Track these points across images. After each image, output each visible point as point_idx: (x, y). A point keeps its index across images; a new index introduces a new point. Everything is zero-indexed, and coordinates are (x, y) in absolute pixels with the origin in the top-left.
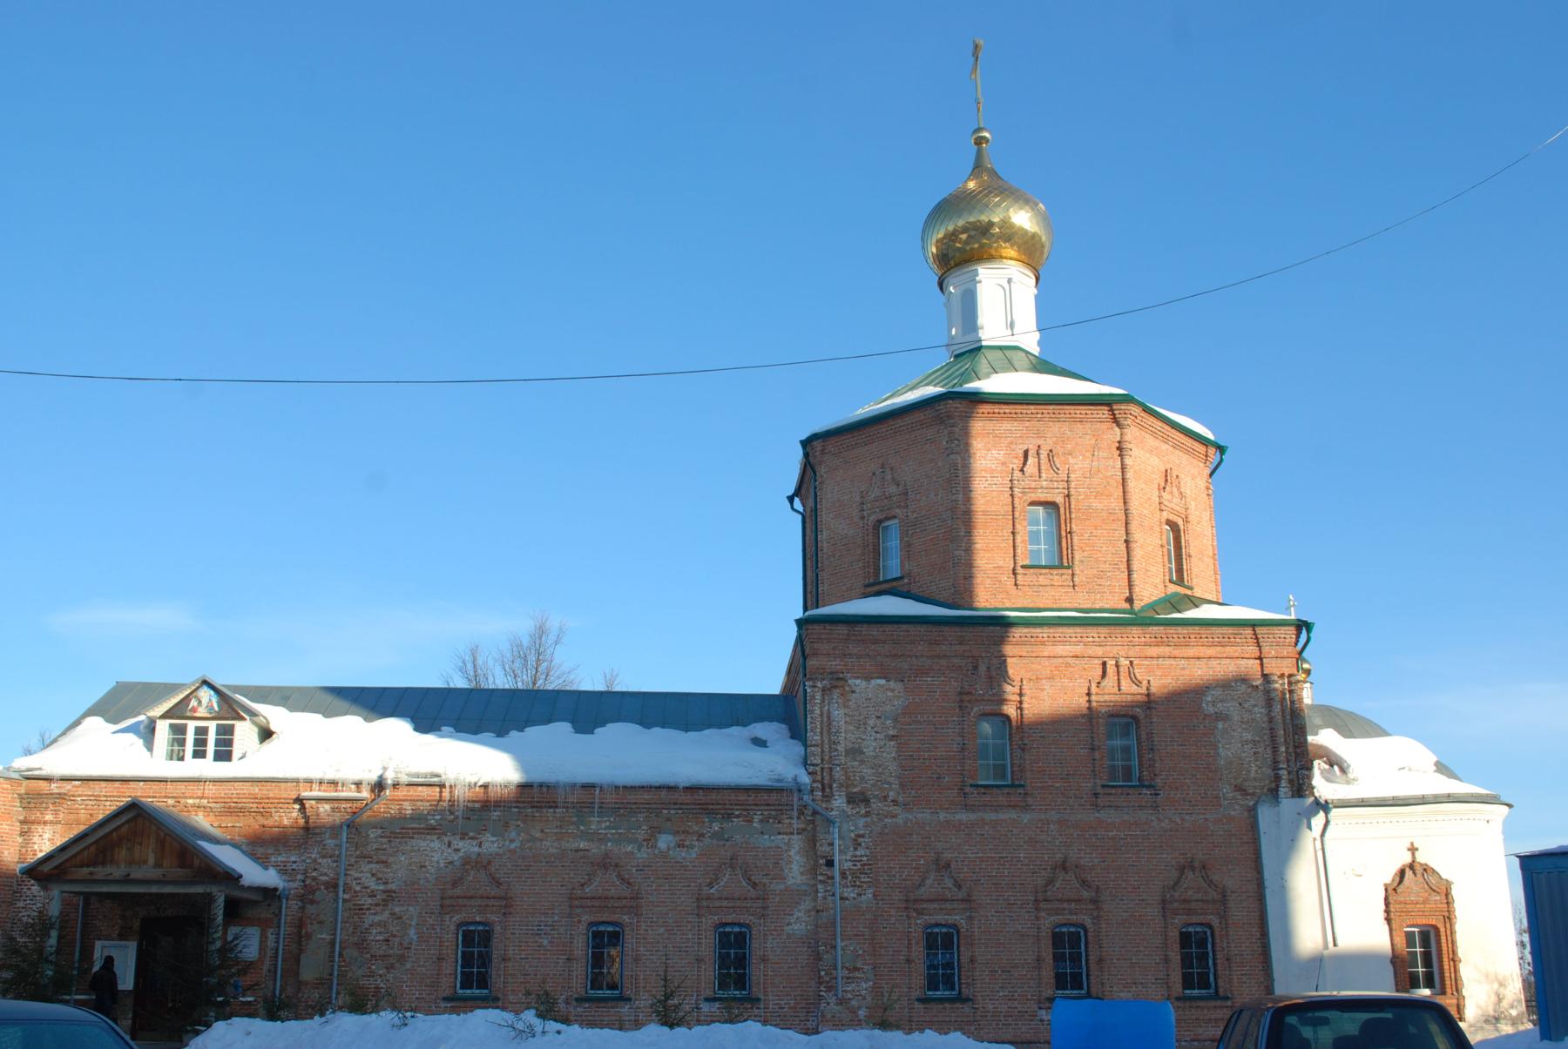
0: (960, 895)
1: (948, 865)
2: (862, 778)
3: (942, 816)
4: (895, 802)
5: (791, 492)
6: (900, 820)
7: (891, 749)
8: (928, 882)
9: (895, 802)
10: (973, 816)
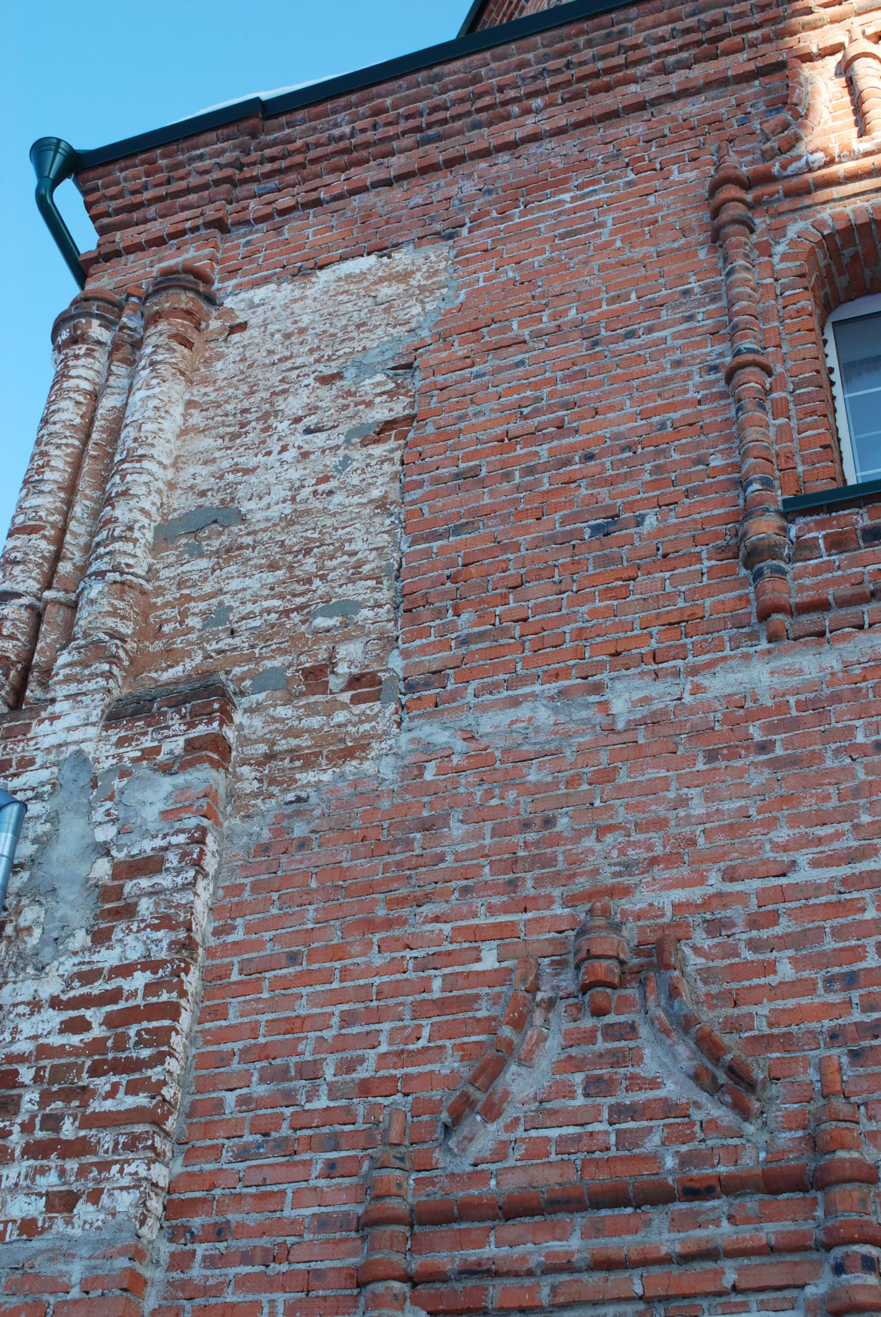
0: (759, 1144)
1: (656, 956)
2: (218, 618)
3: (624, 698)
4: (364, 684)
5: (86, 140)
6: (380, 767)
7: (377, 470)
8: (521, 1084)
9: (364, 684)
10: (813, 664)
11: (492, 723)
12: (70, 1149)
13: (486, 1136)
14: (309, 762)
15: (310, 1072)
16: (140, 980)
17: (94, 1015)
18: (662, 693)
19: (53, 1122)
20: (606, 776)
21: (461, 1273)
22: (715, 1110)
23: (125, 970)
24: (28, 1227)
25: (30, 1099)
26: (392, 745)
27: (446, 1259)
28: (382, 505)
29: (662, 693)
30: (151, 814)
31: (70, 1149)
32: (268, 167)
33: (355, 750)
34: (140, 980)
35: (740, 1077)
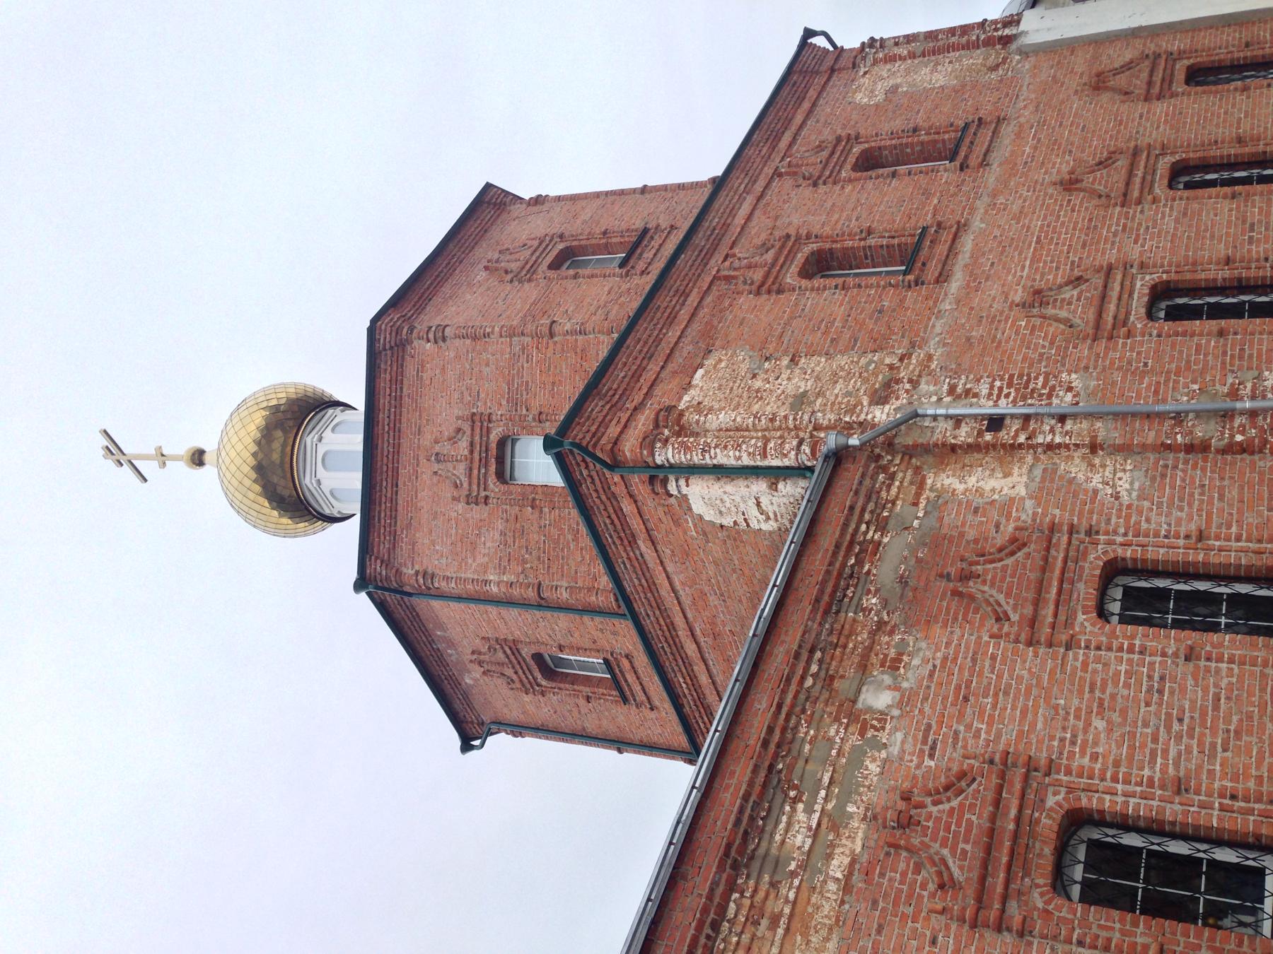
0: (1098, 281)
8: (1063, 314)
12: (1053, 388)
17: (1006, 391)
22: (1084, 287)
23: (992, 387)
27: (1110, 319)
30: (932, 388)
35: (1079, 278)
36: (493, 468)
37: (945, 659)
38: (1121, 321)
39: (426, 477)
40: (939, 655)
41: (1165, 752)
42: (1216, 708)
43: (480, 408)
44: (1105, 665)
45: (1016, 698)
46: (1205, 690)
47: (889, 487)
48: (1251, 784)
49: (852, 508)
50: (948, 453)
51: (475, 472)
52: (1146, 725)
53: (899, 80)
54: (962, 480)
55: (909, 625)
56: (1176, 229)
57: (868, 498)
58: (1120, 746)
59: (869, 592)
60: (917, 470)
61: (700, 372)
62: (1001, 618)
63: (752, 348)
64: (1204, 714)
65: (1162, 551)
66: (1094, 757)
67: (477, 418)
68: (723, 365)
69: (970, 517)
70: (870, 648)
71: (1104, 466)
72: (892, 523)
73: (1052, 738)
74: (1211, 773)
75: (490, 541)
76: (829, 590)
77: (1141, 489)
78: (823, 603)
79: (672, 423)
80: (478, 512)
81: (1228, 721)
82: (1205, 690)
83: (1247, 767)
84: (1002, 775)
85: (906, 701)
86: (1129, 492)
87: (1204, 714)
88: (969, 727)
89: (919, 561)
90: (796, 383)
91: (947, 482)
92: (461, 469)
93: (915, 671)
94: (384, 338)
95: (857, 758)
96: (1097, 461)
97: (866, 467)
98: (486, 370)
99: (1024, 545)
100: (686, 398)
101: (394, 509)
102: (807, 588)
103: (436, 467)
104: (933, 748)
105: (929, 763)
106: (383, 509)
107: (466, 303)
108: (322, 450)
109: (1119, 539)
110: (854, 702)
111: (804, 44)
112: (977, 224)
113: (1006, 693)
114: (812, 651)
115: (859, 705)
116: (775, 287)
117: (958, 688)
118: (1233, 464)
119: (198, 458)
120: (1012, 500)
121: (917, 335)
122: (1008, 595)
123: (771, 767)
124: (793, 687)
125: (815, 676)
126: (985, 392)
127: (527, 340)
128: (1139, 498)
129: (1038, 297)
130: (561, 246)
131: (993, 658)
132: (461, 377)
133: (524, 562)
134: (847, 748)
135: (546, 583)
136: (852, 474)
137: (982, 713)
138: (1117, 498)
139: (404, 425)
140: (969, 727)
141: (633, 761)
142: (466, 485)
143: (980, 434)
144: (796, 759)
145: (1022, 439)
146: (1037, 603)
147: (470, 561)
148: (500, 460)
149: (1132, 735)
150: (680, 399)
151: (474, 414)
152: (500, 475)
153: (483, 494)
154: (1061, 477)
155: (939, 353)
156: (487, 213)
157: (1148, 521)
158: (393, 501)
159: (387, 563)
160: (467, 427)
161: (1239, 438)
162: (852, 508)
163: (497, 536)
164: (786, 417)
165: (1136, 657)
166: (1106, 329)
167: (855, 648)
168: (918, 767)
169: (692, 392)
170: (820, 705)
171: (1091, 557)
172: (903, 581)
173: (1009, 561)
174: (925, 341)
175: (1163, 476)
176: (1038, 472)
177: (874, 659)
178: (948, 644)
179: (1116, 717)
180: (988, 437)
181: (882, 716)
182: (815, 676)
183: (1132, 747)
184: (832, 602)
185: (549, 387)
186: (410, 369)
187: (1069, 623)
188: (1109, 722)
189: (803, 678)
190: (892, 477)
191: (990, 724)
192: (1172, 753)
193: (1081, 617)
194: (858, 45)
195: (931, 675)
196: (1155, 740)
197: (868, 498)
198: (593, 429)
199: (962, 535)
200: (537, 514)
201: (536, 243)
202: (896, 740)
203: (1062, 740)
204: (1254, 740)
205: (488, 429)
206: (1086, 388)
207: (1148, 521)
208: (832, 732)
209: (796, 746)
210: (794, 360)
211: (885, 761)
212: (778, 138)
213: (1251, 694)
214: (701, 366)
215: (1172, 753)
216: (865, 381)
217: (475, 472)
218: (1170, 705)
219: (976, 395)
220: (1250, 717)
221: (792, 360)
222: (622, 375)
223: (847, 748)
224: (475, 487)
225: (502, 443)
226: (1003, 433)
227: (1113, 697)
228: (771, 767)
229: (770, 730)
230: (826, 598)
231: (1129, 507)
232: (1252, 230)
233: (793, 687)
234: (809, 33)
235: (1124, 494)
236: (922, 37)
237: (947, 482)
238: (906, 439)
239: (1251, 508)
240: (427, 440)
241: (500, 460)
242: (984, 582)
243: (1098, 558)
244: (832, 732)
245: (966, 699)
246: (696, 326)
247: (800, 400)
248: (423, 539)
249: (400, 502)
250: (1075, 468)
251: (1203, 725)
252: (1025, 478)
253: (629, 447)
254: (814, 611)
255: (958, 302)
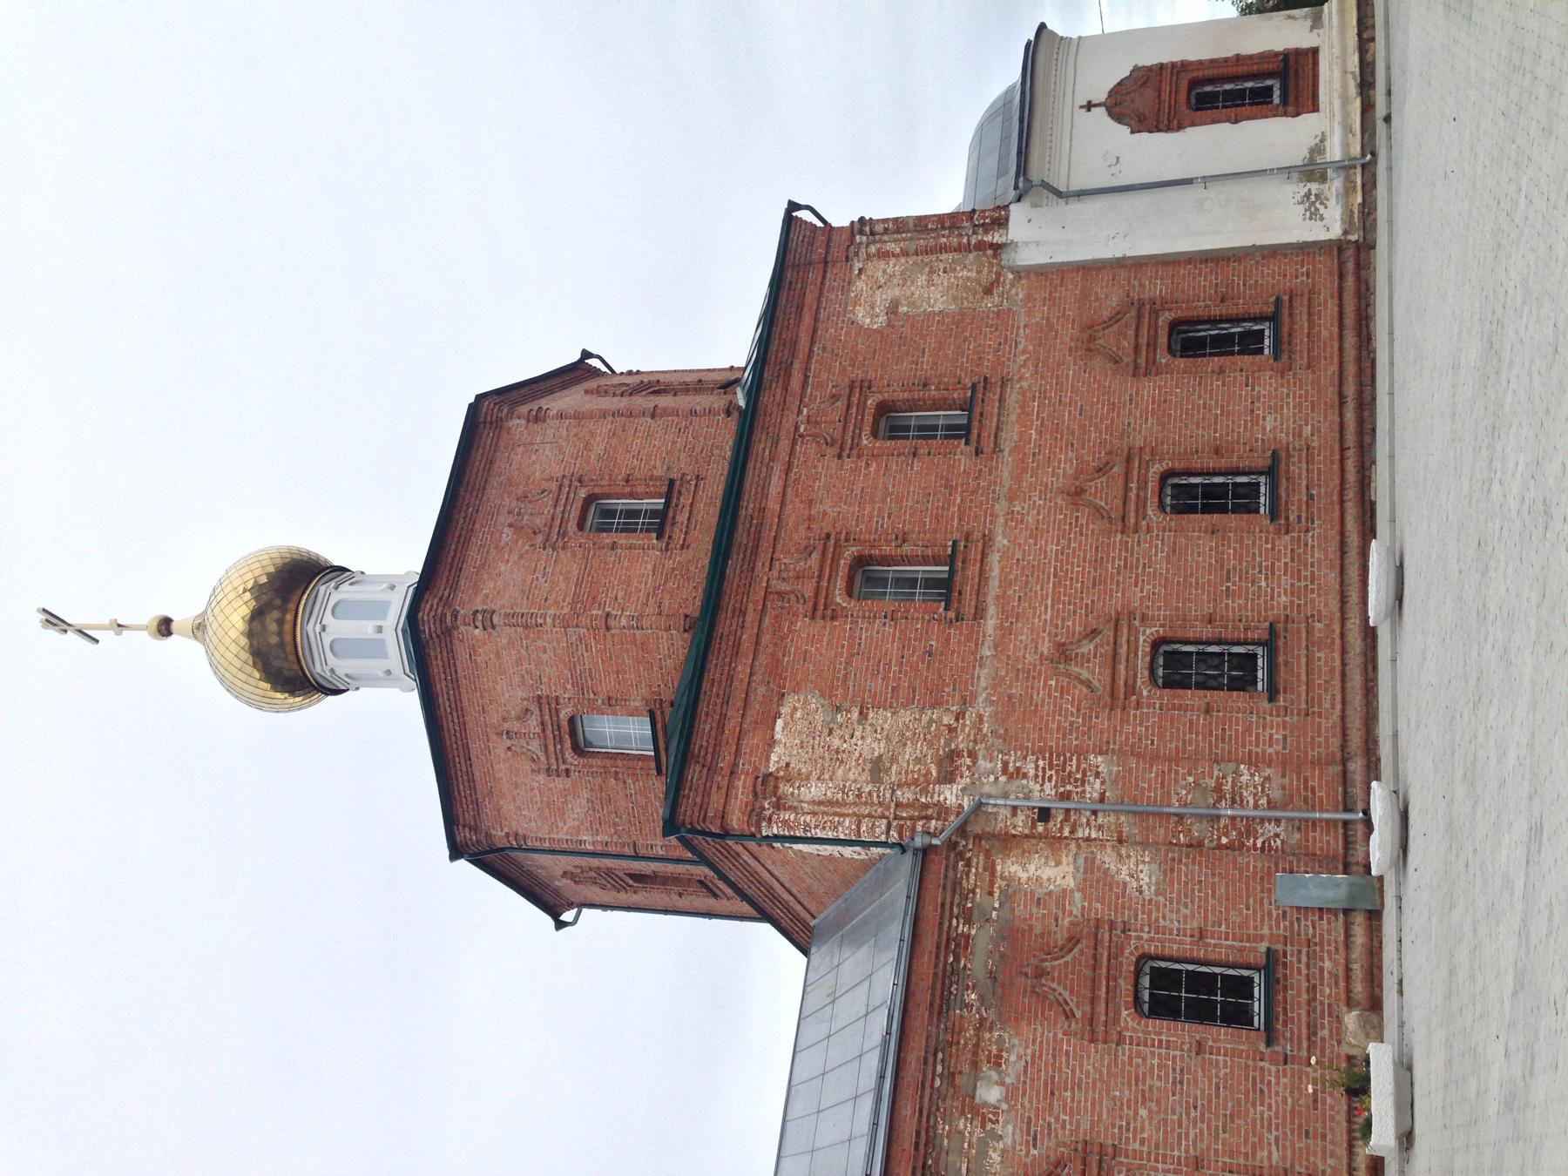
0: (1108, 633)
3: (987, 652)
8: (1085, 675)
10: (992, 610)
11: (983, 683)
12: (1084, 774)
13: (1096, 683)
14: (980, 730)
15: (1072, 724)
16: (1041, 763)
17: (1048, 773)
18: (989, 642)
19: (1076, 780)
20: (1008, 657)
21: (701, 882)
22: (1098, 640)
23: (1037, 767)
24: (1103, 783)
25: (1069, 787)
26: (982, 706)
27: (1122, 690)
28: (894, 713)
29: (989, 642)
30: (989, 765)
31: (1084, 774)
32: (926, 1105)
33: (980, 717)
34: (1041, 763)
35: (1093, 631)
36: (568, 744)
37: (1033, 1055)
38: (1131, 689)
39: (500, 751)
40: (1029, 1051)
41: (1187, 1135)
42: (1217, 1097)
43: (544, 690)
44: (1144, 1059)
45: (1087, 1092)
46: (1210, 1081)
47: (968, 874)
48: (1242, 1161)
49: (943, 905)
50: (1007, 841)
51: (551, 748)
52: (1173, 1113)
53: (897, 292)
54: (1025, 869)
55: (1004, 1021)
56: (1168, 570)
57: (954, 891)
58: (1158, 1130)
59: (968, 987)
60: (988, 853)
61: (780, 723)
62: (1069, 1015)
63: (823, 695)
64: (1210, 1101)
65: (1175, 947)
66: (1142, 1142)
67: (544, 701)
68: (799, 714)
69: (1035, 910)
70: (977, 1046)
71: (1129, 857)
72: (976, 913)
73: (1114, 1126)
74: (1216, 1151)
75: (578, 808)
76: (938, 993)
77: (1157, 883)
78: (936, 1006)
79: (766, 784)
80: (559, 783)
81: (1225, 1109)
82: (1210, 1081)
83: (1238, 1146)
84: (1084, 1163)
85: (1011, 1094)
86: (1149, 885)
87: (1210, 1101)
88: (1057, 1119)
89: (1002, 955)
90: (871, 746)
91: (1013, 869)
92: (535, 745)
93: (1014, 1063)
94: (428, 627)
95: (983, 1146)
96: (1123, 851)
97: (947, 858)
98: (545, 657)
99: (1078, 941)
100: (774, 758)
101: (471, 780)
102: (923, 996)
103: (509, 743)
104: (1035, 1139)
105: (1034, 1152)
106: (462, 787)
107: (505, 576)
108: (327, 639)
109: (1145, 936)
110: (973, 1097)
111: (790, 221)
112: (1001, 541)
113: (1080, 1087)
114: (935, 1055)
115: (977, 1100)
116: (829, 612)
117: (1046, 1083)
118: (1221, 859)
119: (165, 627)
120: (1064, 891)
121: (966, 689)
122: (1072, 992)
123: (924, 1164)
124: (928, 1091)
125: (941, 1076)
126: (1032, 772)
127: (583, 631)
128: (1158, 893)
129: (1063, 653)
130: (583, 494)
131: (1067, 1053)
132: (519, 662)
133: (615, 824)
134: (974, 1140)
135: (640, 842)
136: (938, 866)
137: (1065, 1105)
138: (1141, 893)
139: (466, 704)
140: (1057, 1119)
141: (715, 921)
142: (543, 759)
143: (1034, 826)
144: (940, 1153)
145: (1066, 833)
146: (1093, 1001)
147: (560, 824)
148: (573, 734)
149: (1165, 1120)
150: (768, 759)
151: (540, 697)
152: (576, 748)
153: (563, 767)
154: (1099, 868)
155: (987, 712)
156: (487, 436)
157: (1164, 918)
158: (469, 773)
159: (474, 829)
160: (534, 708)
161: (1224, 840)
162: (943, 905)
163: (584, 802)
164: (870, 793)
165: (1163, 1051)
166: (1119, 697)
167: (966, 1044)
168: (1027, 1155)
169: (778, 749)
170: (948, 1102)
171: (1127, 952)
172: (992, 976)
173: (1069, 958)
174: (974, 696)
175: (1172, 870)
176: (1081, 861)
177: (983, 1057)
178: (1034, 1041)
179: (1154, 1106)
180: (1040, 827)
181: (995, 1109)
182: (941, 1076)
183: (1166, 1132)
184: (942, 1004)
185: (613, 676)
186: (462, 655)
187: (1116, 1021)
188: (1150, 1111)
189: (933, 1080)
190: (968, 864)
191: (1071, 1116)
192: (1191, 1137)
193: (1125, 1013)
194: (846, 224)
195: (1026, 1068)
196: (1180, 1126)
197: (954, 891)
198: (698, 800)
199: (1031, 928)
200: (621, 785)
201: (554, 486)
202: (1008, 1131)
203: (1121, 1127)
204: (1242, 1122)
205: (557, 712)
206: (1110, 773)
207: (1164, 918)
208: (961, 1126)
209: (937, 1142)
210: (863, 715)
211: (1003, 1151)
212: (788, 374)
213: (1239, 1084)
214: (778, 715)
215: (1191, 1137)
216: (930, 745)
217: (551, 748)
218: (1188, 1095)
219: (1025, 776)
220: (1239, 1101)
221: (861, 713)
222: (708, 727)
223: (974, 1140)
224: (553, 761)
225: (572, 721)
226: (1051, 824)
227: (1151, 1087)
228: (924, 1164)
229: (918, 1133)
230: (938, 1001)
231: (1150, 901)
232: (1228, 579)
233: (928, 1091)
234: (793, 206)
235: (1145, 887)
236: (911, 225)
237: (1013, 869)
238: (975, 828)
239: (1234, 908)
240: (494, 718)
241: (573, 734)
242: (1053, 980)
243: (1131, 953)
244: (961, 1126)
245: (1052, 1093)
246: (763, 659)
247: (877, 768)
248: (507, 807)
249: (477, 773)
250: (1108, 858)
251: (1210, 1112)
252: (1071, 869)
253: (736, 821)
254: (931, 1014)
255: (996, 646)
